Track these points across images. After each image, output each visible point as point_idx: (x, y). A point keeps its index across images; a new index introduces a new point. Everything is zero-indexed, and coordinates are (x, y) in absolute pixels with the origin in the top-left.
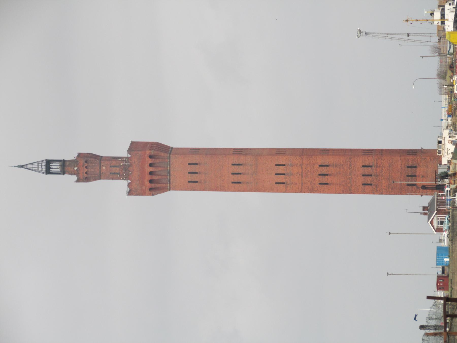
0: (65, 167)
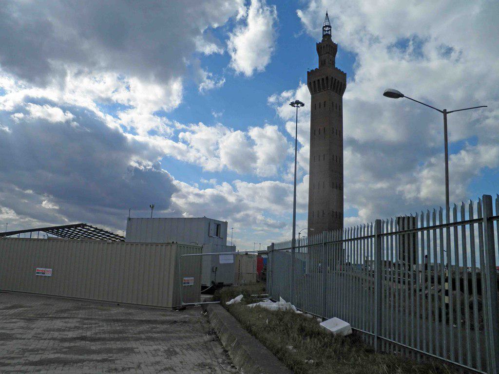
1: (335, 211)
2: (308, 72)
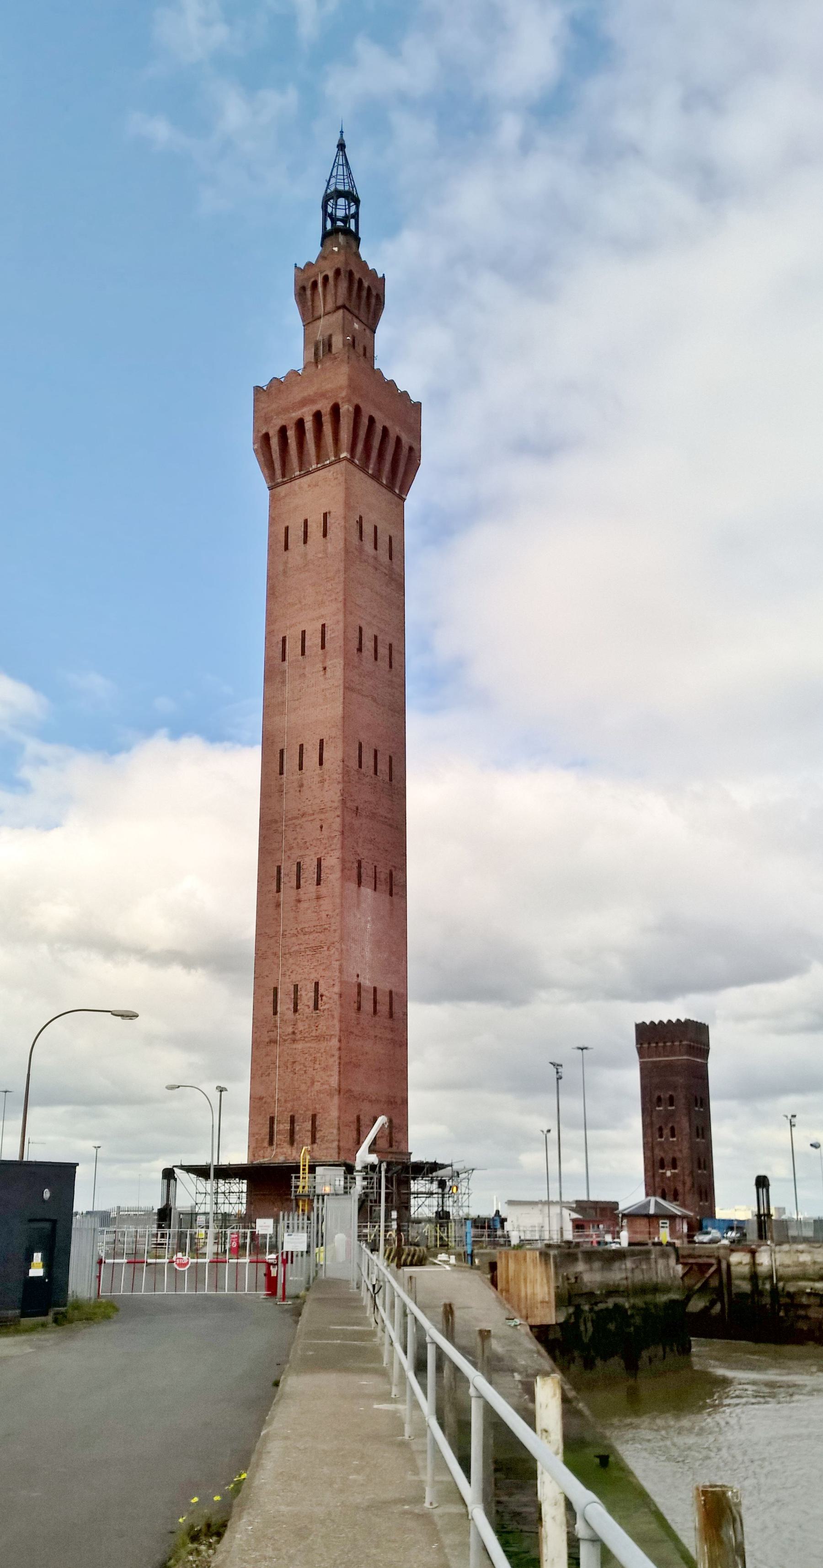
0: (341, 139)
1: (367, 983)
2: (258, 389)
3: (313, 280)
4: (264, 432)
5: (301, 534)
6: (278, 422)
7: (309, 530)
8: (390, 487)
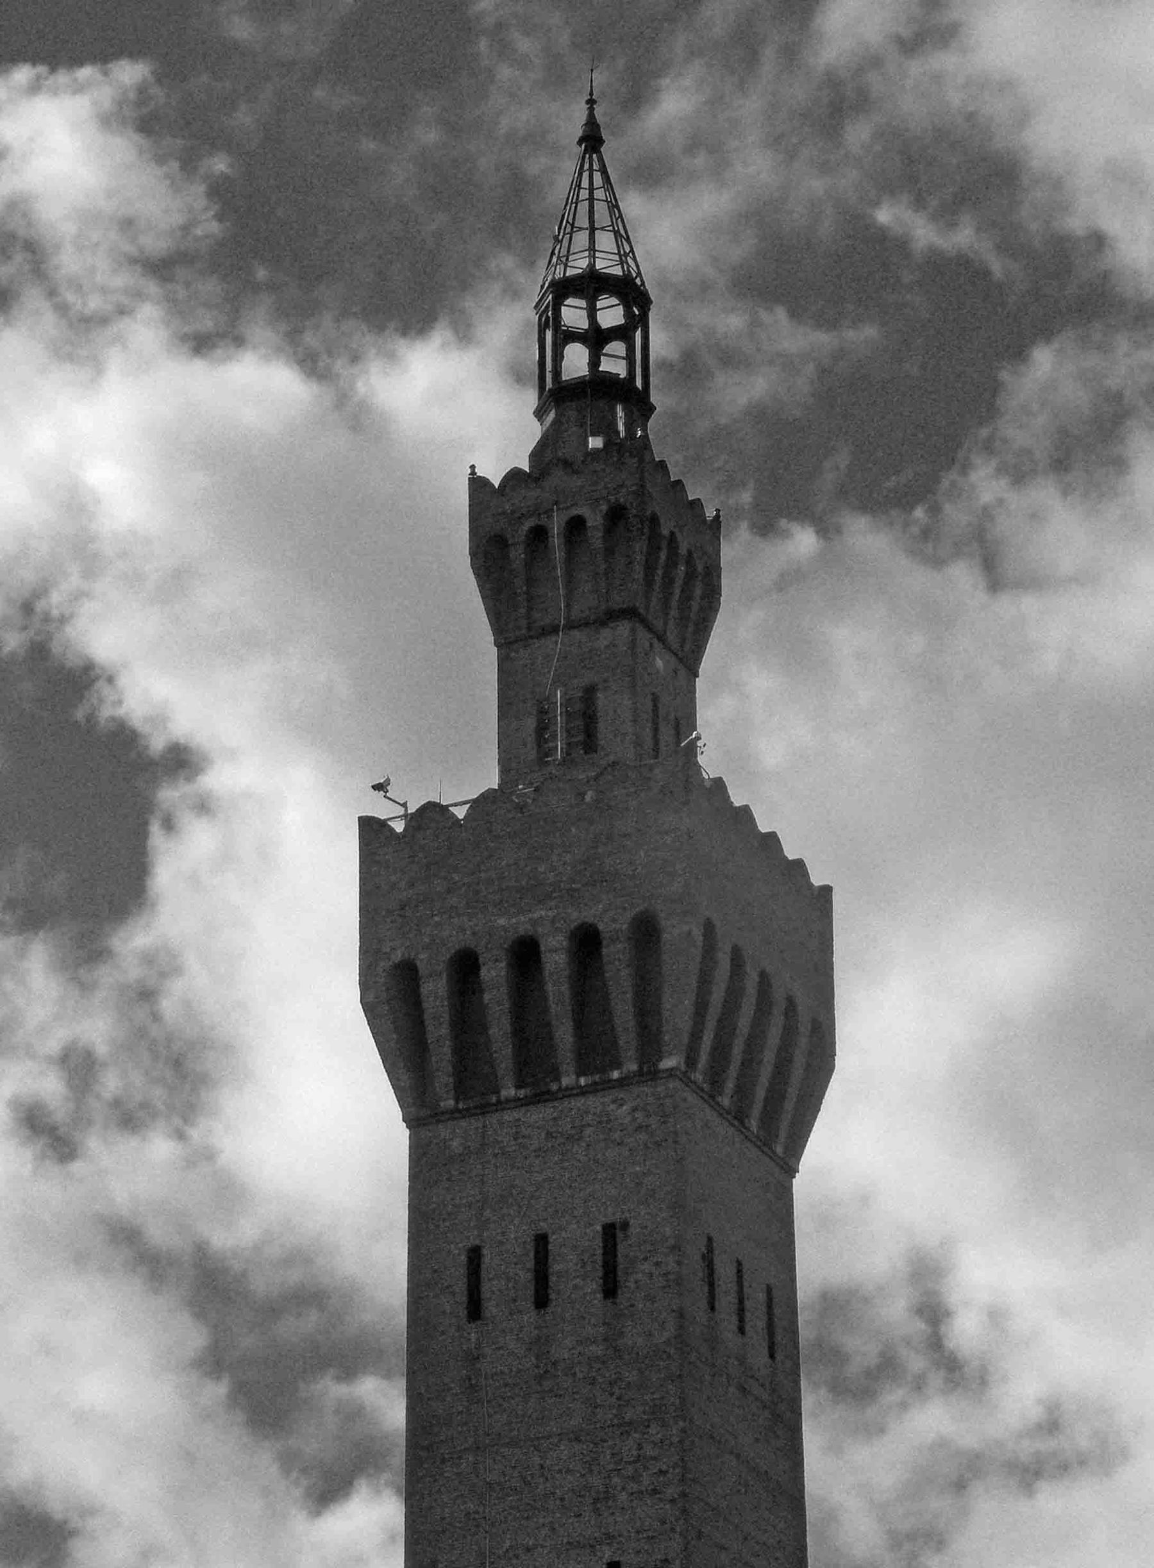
3: (528, 525)
4: (398, 956)
5: (525, 1276)
6: (455, 934)
7: (555, 1267)
8: (765, 1143)
